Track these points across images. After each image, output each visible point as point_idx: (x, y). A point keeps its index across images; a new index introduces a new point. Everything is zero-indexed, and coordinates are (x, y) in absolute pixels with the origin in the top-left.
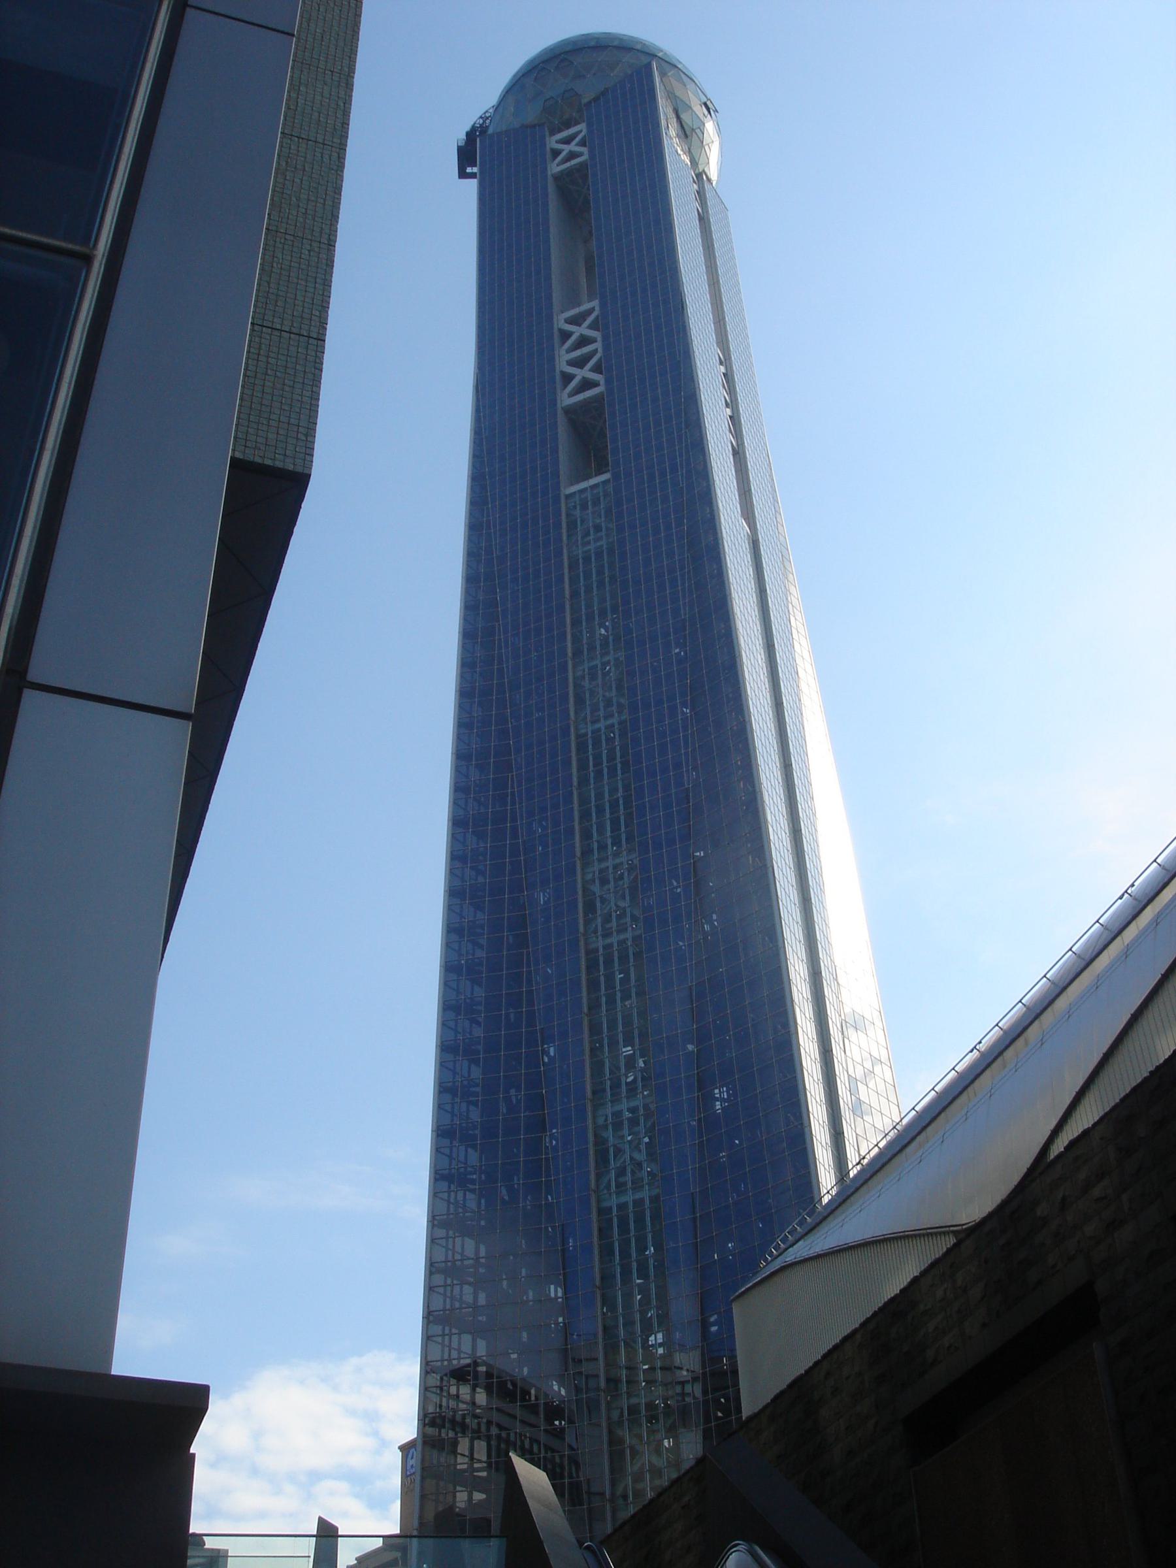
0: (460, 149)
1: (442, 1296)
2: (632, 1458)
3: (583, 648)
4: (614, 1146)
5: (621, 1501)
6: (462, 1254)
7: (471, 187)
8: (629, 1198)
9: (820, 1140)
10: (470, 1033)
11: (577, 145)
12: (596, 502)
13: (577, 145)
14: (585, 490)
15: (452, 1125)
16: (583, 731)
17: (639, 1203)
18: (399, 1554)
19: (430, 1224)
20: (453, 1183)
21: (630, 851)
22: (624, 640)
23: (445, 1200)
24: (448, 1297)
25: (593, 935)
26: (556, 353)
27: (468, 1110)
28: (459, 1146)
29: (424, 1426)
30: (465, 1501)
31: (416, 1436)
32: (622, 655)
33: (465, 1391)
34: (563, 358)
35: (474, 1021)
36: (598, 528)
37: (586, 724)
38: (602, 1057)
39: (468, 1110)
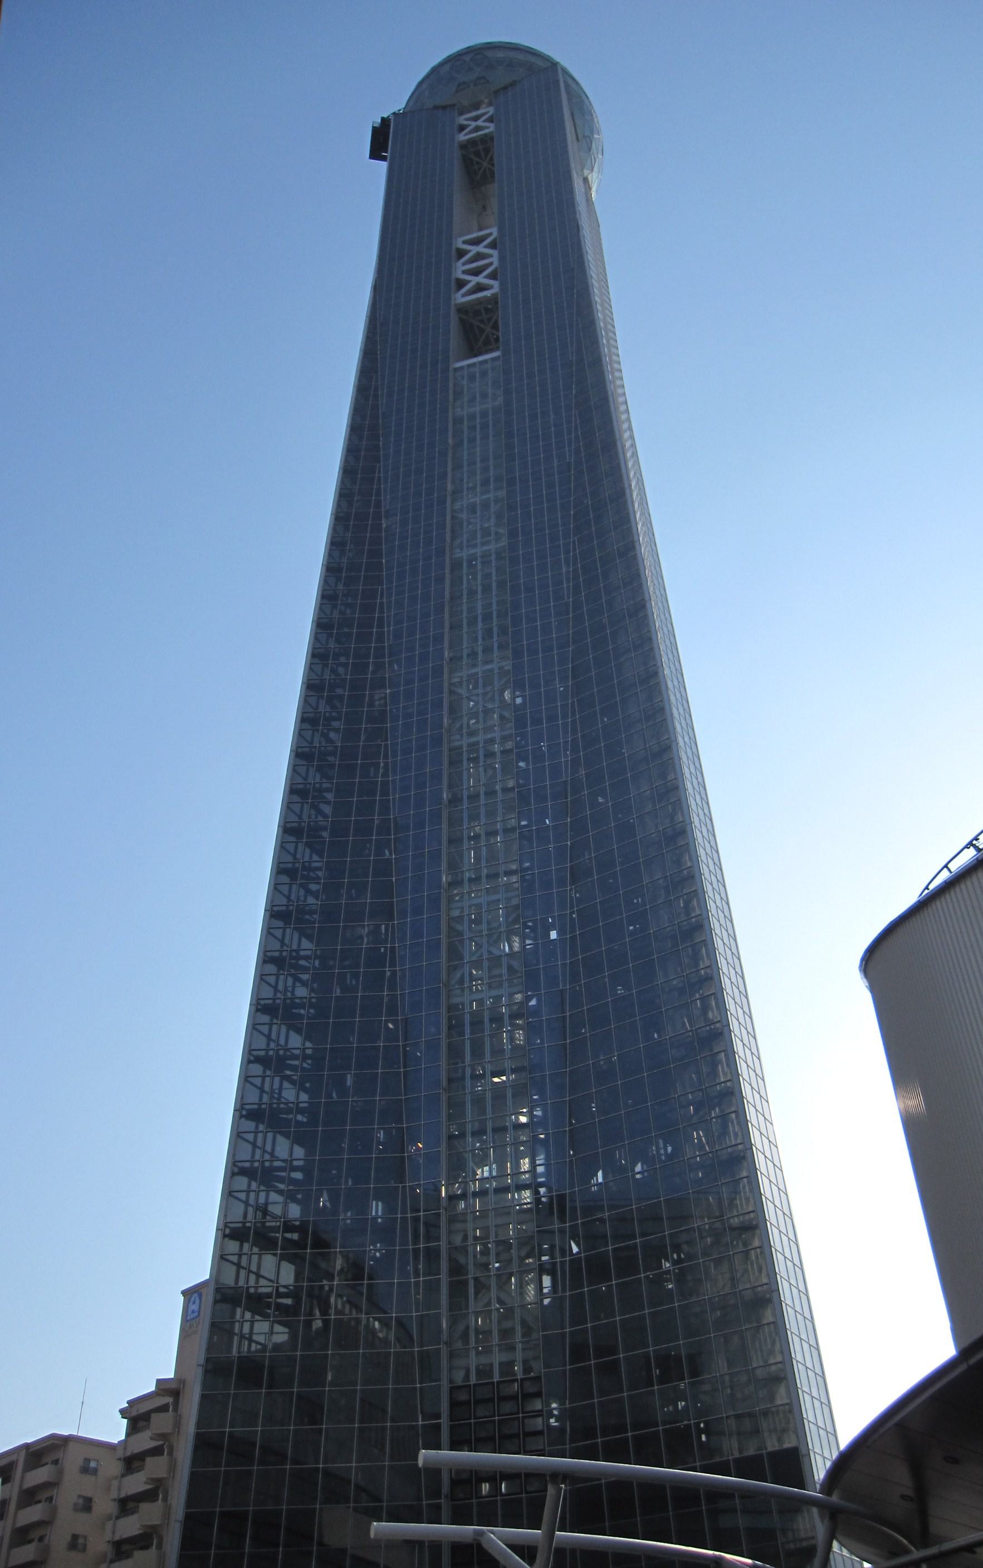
0: (375, 130)
1: (279, 943)
2: (476, 1294)
3: (462, 795)
4: (476, 1279)
5: (459, 1345)
6: (272, 1154)
7: (382, 167)
8: (477, 409)
9: (759, 1115)
10: (293, 992)
11: (486, 277)
12: (484, 374)
13: (486, 277)
14: (474, 365)
15: (305, 784)
16: (457, 744)
17: (484, 414)
18: (169, 1400)
19: (238, 1113)
20: (255, 1180)
21: (496, 489)
22: (512, 616)
23: (279, 940)
24: (251, 1206)
25: (457, 987)
26: (453, 265)
27: (281, 1088)
28: (281, 1024)
29: (223, 1238)
30: (266, 1334)
31: (208, 1277)
32: (508, 665)
33: (269, 1262)
34: (459, 269)
35: (302, 933)
36: (486, 532)
37: (462, 736)
38: (461, 1150)
39: (281, 1088)
